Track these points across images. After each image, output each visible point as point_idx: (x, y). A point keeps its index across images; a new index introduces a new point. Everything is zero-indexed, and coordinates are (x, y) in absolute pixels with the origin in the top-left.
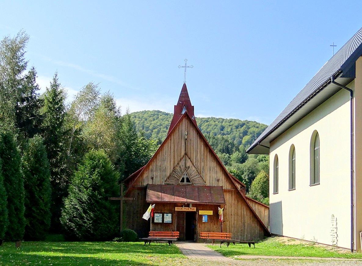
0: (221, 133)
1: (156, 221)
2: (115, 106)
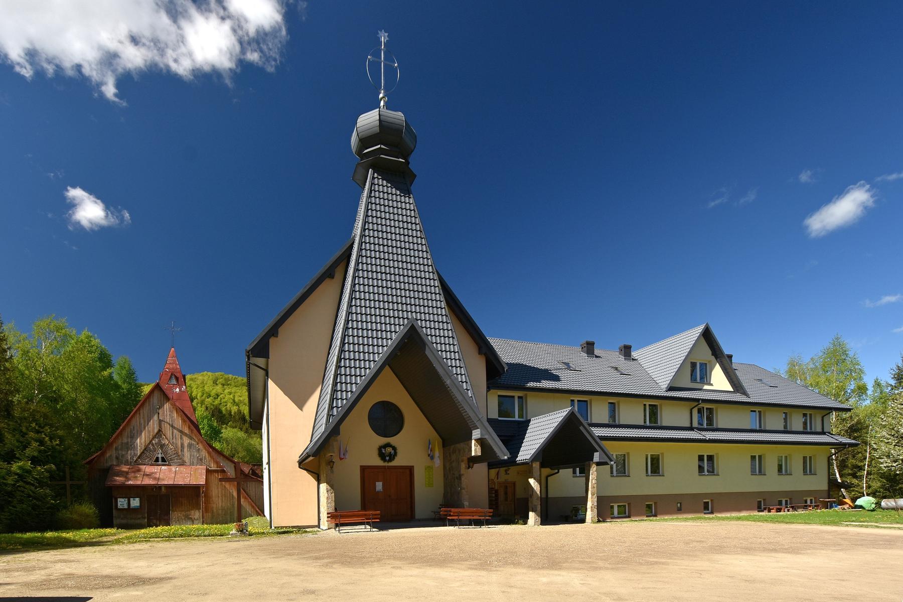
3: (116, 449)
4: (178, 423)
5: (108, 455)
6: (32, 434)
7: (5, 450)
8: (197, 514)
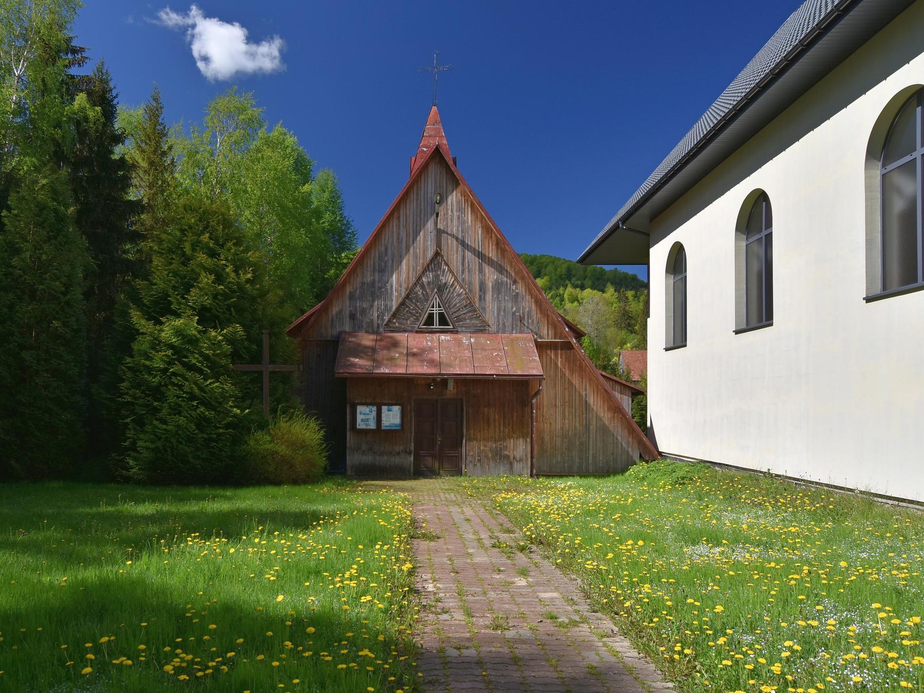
3: (352, 297)
4: (476, 236)
5: (335, 310)
6: (202, 257)
7: (152, 296)
8: (519, 448)
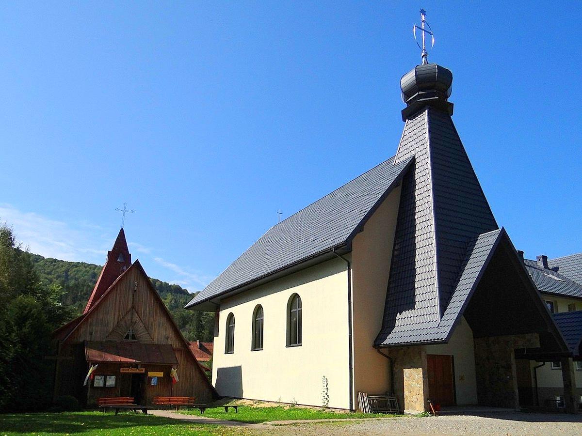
0: (92, 281)
1: (96, 385)
2: (14, 242)
5: (82, 330)
